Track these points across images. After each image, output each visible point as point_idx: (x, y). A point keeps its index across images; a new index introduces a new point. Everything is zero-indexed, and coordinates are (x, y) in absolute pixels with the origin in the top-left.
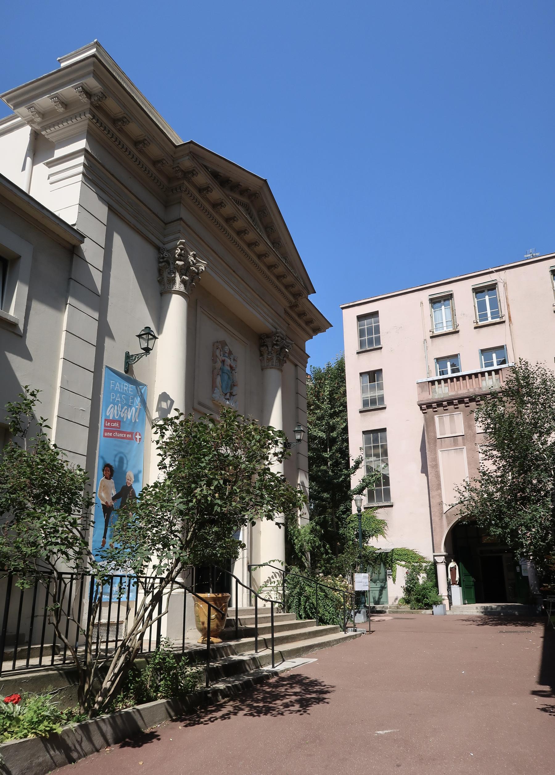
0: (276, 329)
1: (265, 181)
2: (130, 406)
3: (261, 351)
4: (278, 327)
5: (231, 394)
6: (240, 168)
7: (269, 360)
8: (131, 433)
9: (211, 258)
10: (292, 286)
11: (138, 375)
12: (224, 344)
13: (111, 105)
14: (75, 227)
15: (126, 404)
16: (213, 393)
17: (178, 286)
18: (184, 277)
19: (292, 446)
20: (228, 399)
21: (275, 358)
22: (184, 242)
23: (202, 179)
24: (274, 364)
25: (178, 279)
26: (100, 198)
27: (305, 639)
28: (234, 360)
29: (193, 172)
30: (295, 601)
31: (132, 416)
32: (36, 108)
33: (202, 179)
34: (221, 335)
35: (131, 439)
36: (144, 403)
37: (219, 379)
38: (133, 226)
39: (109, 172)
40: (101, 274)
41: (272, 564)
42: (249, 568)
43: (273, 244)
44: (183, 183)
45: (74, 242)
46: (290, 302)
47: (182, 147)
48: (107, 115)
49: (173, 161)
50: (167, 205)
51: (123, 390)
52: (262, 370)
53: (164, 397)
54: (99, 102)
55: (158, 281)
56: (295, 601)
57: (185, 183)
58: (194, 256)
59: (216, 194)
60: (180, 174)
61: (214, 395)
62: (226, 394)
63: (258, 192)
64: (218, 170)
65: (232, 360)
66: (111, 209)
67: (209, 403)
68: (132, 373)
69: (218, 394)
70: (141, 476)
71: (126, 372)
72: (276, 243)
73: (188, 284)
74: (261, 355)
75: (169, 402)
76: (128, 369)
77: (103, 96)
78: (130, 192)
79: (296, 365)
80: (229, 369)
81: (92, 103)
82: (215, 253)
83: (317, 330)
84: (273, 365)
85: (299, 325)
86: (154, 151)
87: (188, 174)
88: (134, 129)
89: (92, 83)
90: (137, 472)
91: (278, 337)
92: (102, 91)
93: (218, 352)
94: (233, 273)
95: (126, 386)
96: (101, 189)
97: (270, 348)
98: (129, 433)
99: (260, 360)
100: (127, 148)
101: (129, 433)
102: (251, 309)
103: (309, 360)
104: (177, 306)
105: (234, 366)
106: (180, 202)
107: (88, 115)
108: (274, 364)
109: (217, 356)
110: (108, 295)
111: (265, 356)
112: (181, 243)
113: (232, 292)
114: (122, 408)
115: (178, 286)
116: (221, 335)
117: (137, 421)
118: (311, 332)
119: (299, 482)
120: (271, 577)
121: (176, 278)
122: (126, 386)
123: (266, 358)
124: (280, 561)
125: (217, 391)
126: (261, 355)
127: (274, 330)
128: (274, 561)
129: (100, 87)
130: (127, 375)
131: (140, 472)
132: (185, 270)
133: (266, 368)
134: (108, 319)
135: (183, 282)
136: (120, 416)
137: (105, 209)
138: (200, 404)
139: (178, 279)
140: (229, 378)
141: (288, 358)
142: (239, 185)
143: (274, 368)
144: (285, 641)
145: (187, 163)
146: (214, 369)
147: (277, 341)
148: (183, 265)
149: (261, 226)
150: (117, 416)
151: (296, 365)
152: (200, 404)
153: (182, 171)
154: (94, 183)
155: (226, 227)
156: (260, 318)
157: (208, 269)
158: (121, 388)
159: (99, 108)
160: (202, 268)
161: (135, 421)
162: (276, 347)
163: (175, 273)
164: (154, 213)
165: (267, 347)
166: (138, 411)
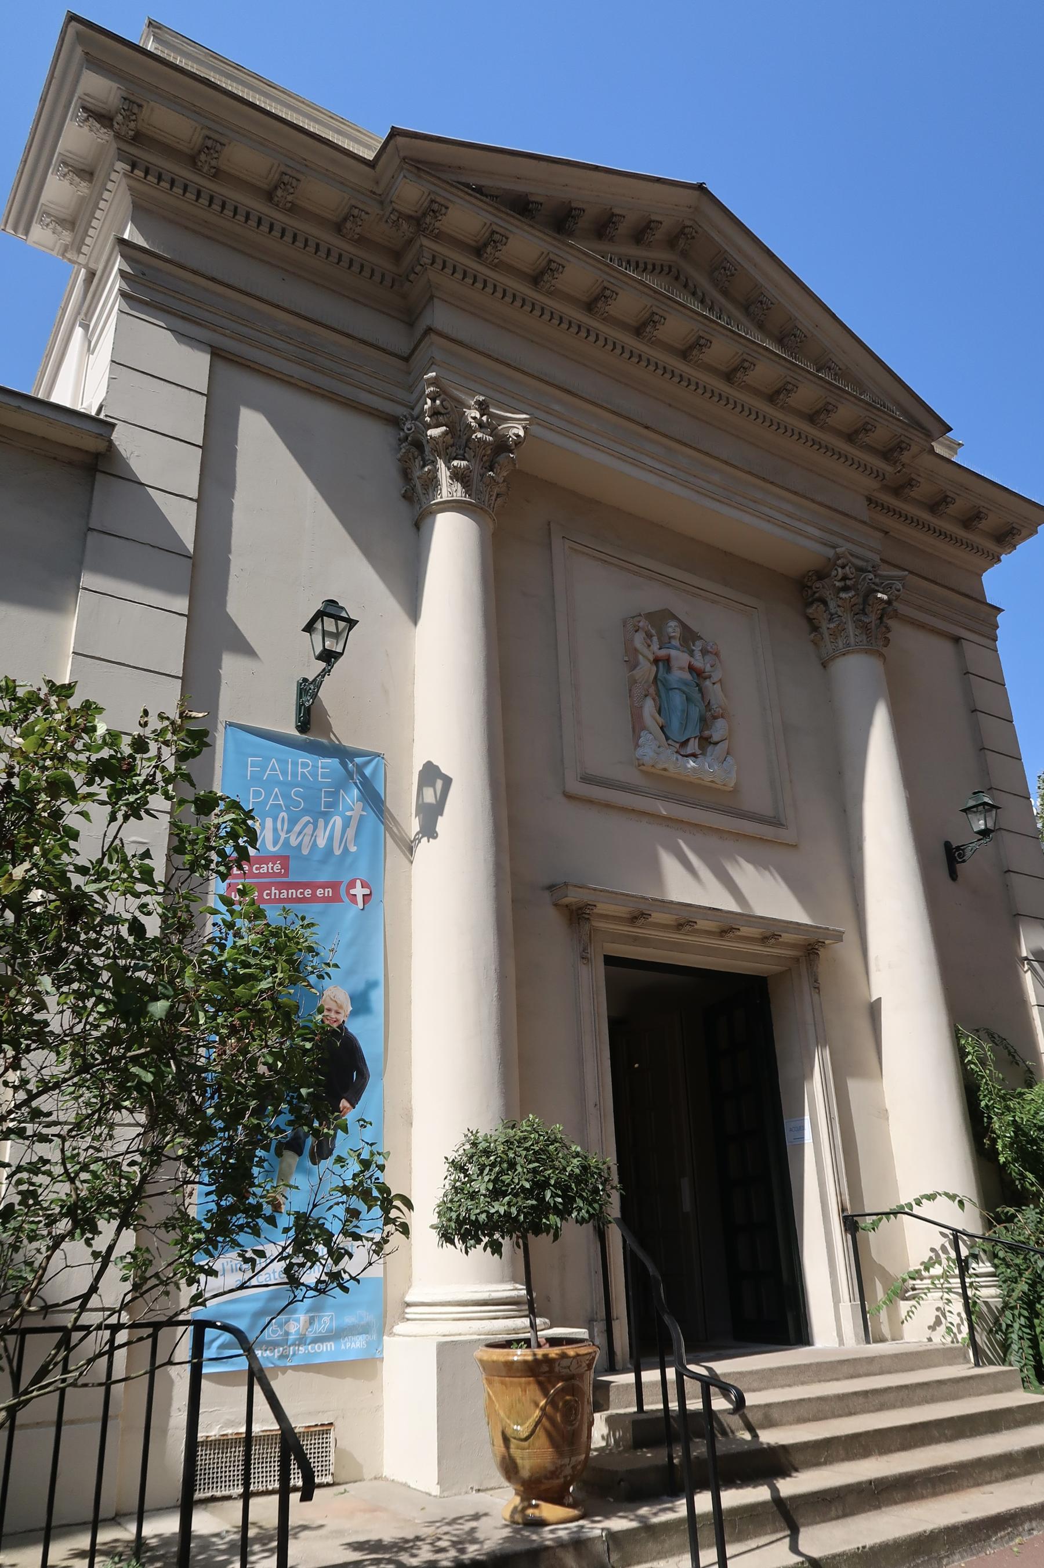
0: (834, 547)
1: (701, 188)
2: (326, 816)
3: (810, 620)
4: (840, 541)
5: (706, 742)
6: (596, 168)
7: (834, 635)
8: (335, 886)
9: (557, 407)
10: (866, 428)
11: (344, 733)
12: (659, 618)
13: (166, 121)
14: (102, 416)
15: (306, 811)
16: (637, 745)
17: (448, 489)
18: (455, 463)
19: (968, 853)
20: (694, 755)
21: (850, 628)
22: (436, 378)
23: (466, 218)
24: (852, 640)
25: (444, 473)
26: (182, 336)
27: (1008, 1477)
28: (704, 652)
29: (434, 209)
30: (1016, 1326)
31: (331, 838)
32: (52, 212)
33: (466, 218)
34: (652, 597)
35: (336, 898)
36: (374, 799)
37: (649, 707)
38: (304, 385)
39: (203, 276)
40: (195, 504)
41: (926, 1209)
42: (851, 1224)
43: (780, 341)
44: (421, 246)
45: (91, 444)
46: (878, 475)
47: (384, 157)
48: (169, 150)
49: (382, 203)
50: (409, 316)
51: (295, 774)
52: (824, 665)
53: (430, 773)
54: (132, 125)
55: (404, 496)
56: (1016, 1326)
57: (426, 242)
58: (483, 407)
59: (526, 244)
60: (405, 226)
61: (640, 752)
62: (684, 744)
63: (688, 223)
64: (521, 188)
65: (698, 654)
66: (217, 354)
67: (635, 778)
68: (327, 729)
69: (651, 748)
70: (377, 997)
71: (304, 726)
72: (788, 337)
73: (475, 476)
74: (815, 628)
75: (439, 783)
76: (308, 716)
77: (131, 105)
78: (278, 307)
79: (957, 640)
80: (687, 676)
81: (118, 136)
82: (569, 392)
83: (1007, 537)
84: (848, 645)
85: (942, 534)
86: (322, 195)
87: (423, 220)
88: (244, 158)
89: (96, 85)
90: (361, 986)
91: (843, 567)
92: (125, 95)
93: (639, 640)
94: (645, 432)
95: (305, 765)
96: (183, 318)
97: (832, 605)
98: (324, 885)
99: (814, 643)
100: (665, 368)
101: (324, 885)
102: (747, 519)
103: (1000, 618)
104: (452, 542)
105: (708, 668)
106: (432, 297)
107: (120, 166)
108: (852, 640)
109: (636, 650)
110: (229, 551)
111: (825, 626)
112: (433, 382)
113: (653, 479)
114: (293, 822)
115: (448, 489)
116: (652, 597)
117: (353, 849)
118: (990, 545)
119: (1024, 954)
120: (938, 1248)
121: (439, 473)
122: (305, 765)
123: (826, 635)
124: (952, 1197)
125: (645, 737)
126: (815, 628)
127: (830, 553)
128: (931, 1197)
129: (115, 85)
130: (304, 736)
131: (372, 985)
132: (458, 442)
133: (833, 658)
134: (233, 608)
135: (457, 476)
136: (287, 841)
137: (202, 360)
138: (587, 779)
139: (444, 473)
140: (688, 699)
141: (896, 615)
142: (613, 215)
143: (853, 652)
144: (898, 1496)
145: (411, 193)
146: (633, 682)
147: (844, 578)
148: (445, 433)
149: (730, 307)
150: (275, 844)
151: (957, 640)
152: (587, 779)
153: (409, 218)
154: (156, 307)
155: (595, 324)
156: (779, 531)
157: (535, 430)
158: (284, 773)
159: (138, 138)
160: (515, 431)
161: (346, 850)
162: (843, 595)
163: (434, 463)
164: (371, 345)
165: (825, 603)
166: (354, 824)
